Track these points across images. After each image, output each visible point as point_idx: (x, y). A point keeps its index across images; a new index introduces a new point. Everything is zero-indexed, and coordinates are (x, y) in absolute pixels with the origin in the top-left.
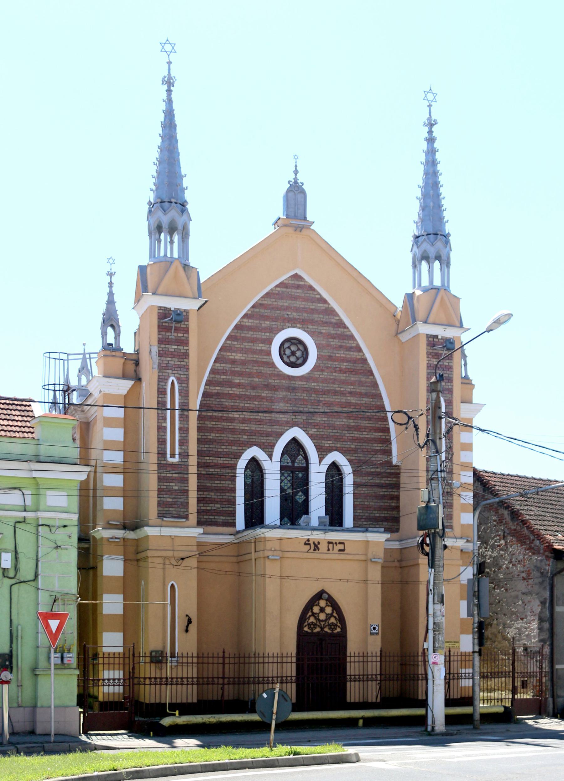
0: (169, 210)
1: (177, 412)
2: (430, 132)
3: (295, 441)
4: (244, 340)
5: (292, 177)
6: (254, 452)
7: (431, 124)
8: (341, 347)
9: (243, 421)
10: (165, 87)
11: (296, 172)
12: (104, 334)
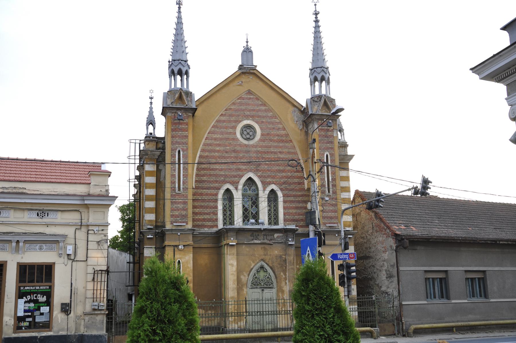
0: (179, 68)
1: (182, 165)
2: (316, 18)
3: (250, 179)
4: (221, 127)
5: (245, 44)
7: (316, 14)
8: (274, 128)
9: (221, 170)
10: (178, 6)
11: (247, 42)
12: (147, 128)
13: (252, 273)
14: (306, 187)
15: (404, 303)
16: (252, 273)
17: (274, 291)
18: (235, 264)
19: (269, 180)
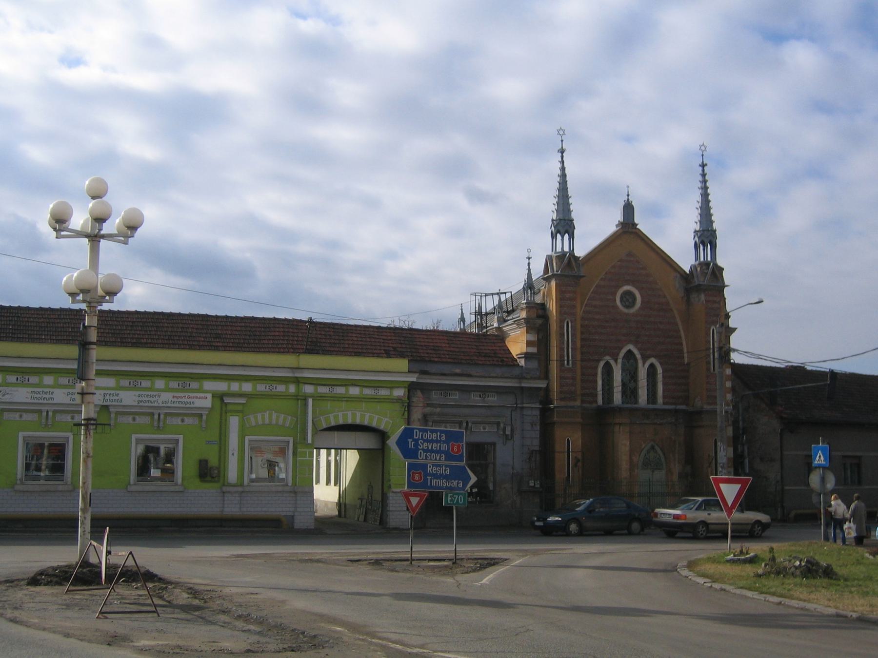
0: (564, 225)
2: (703, 170)
3: (630, 351)
6: (607, 358)
7: (703, 165)
11: (628, 195)
13: (643, 454)
14: (686, 361)
15: (787, 488)
16: (643, 454)
17: (664, 472)
18: (628, 444)
19: (649, 352)
